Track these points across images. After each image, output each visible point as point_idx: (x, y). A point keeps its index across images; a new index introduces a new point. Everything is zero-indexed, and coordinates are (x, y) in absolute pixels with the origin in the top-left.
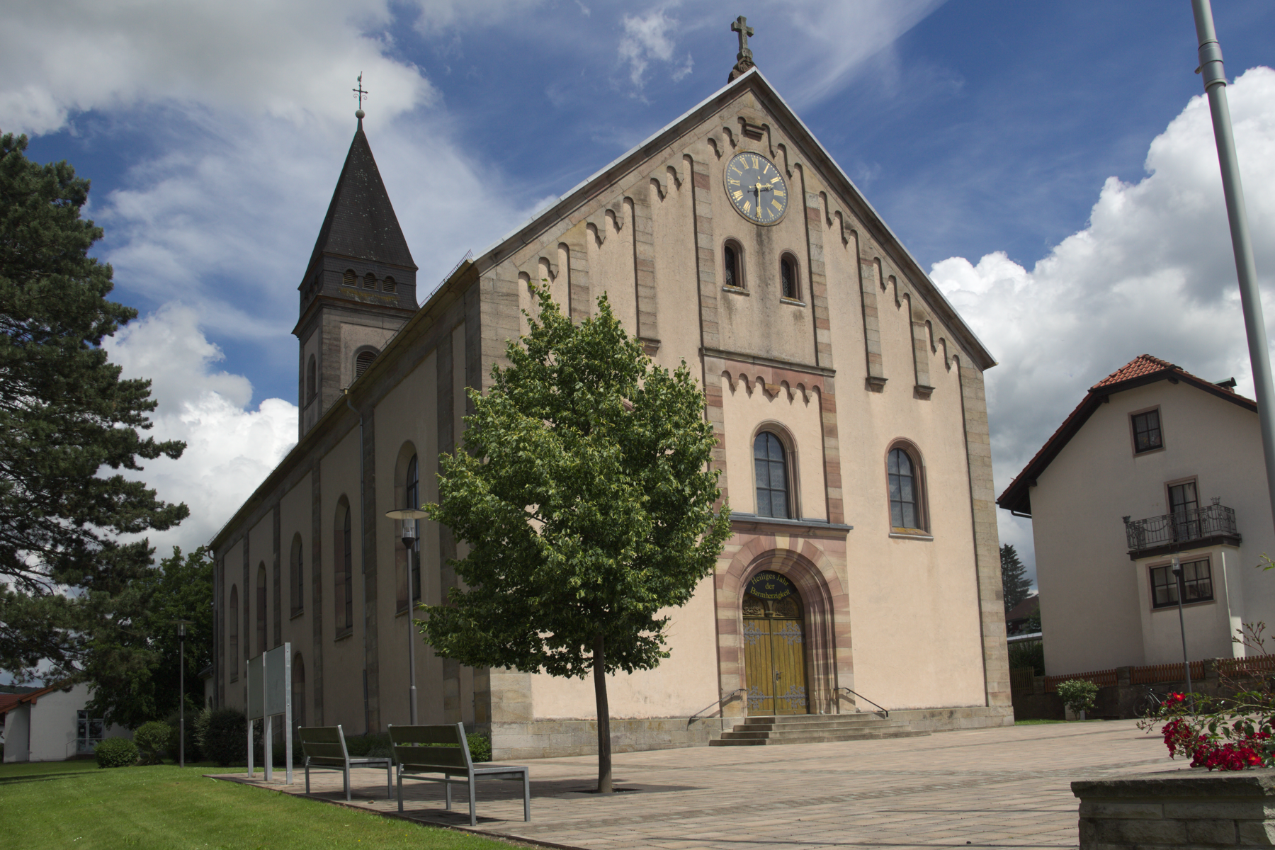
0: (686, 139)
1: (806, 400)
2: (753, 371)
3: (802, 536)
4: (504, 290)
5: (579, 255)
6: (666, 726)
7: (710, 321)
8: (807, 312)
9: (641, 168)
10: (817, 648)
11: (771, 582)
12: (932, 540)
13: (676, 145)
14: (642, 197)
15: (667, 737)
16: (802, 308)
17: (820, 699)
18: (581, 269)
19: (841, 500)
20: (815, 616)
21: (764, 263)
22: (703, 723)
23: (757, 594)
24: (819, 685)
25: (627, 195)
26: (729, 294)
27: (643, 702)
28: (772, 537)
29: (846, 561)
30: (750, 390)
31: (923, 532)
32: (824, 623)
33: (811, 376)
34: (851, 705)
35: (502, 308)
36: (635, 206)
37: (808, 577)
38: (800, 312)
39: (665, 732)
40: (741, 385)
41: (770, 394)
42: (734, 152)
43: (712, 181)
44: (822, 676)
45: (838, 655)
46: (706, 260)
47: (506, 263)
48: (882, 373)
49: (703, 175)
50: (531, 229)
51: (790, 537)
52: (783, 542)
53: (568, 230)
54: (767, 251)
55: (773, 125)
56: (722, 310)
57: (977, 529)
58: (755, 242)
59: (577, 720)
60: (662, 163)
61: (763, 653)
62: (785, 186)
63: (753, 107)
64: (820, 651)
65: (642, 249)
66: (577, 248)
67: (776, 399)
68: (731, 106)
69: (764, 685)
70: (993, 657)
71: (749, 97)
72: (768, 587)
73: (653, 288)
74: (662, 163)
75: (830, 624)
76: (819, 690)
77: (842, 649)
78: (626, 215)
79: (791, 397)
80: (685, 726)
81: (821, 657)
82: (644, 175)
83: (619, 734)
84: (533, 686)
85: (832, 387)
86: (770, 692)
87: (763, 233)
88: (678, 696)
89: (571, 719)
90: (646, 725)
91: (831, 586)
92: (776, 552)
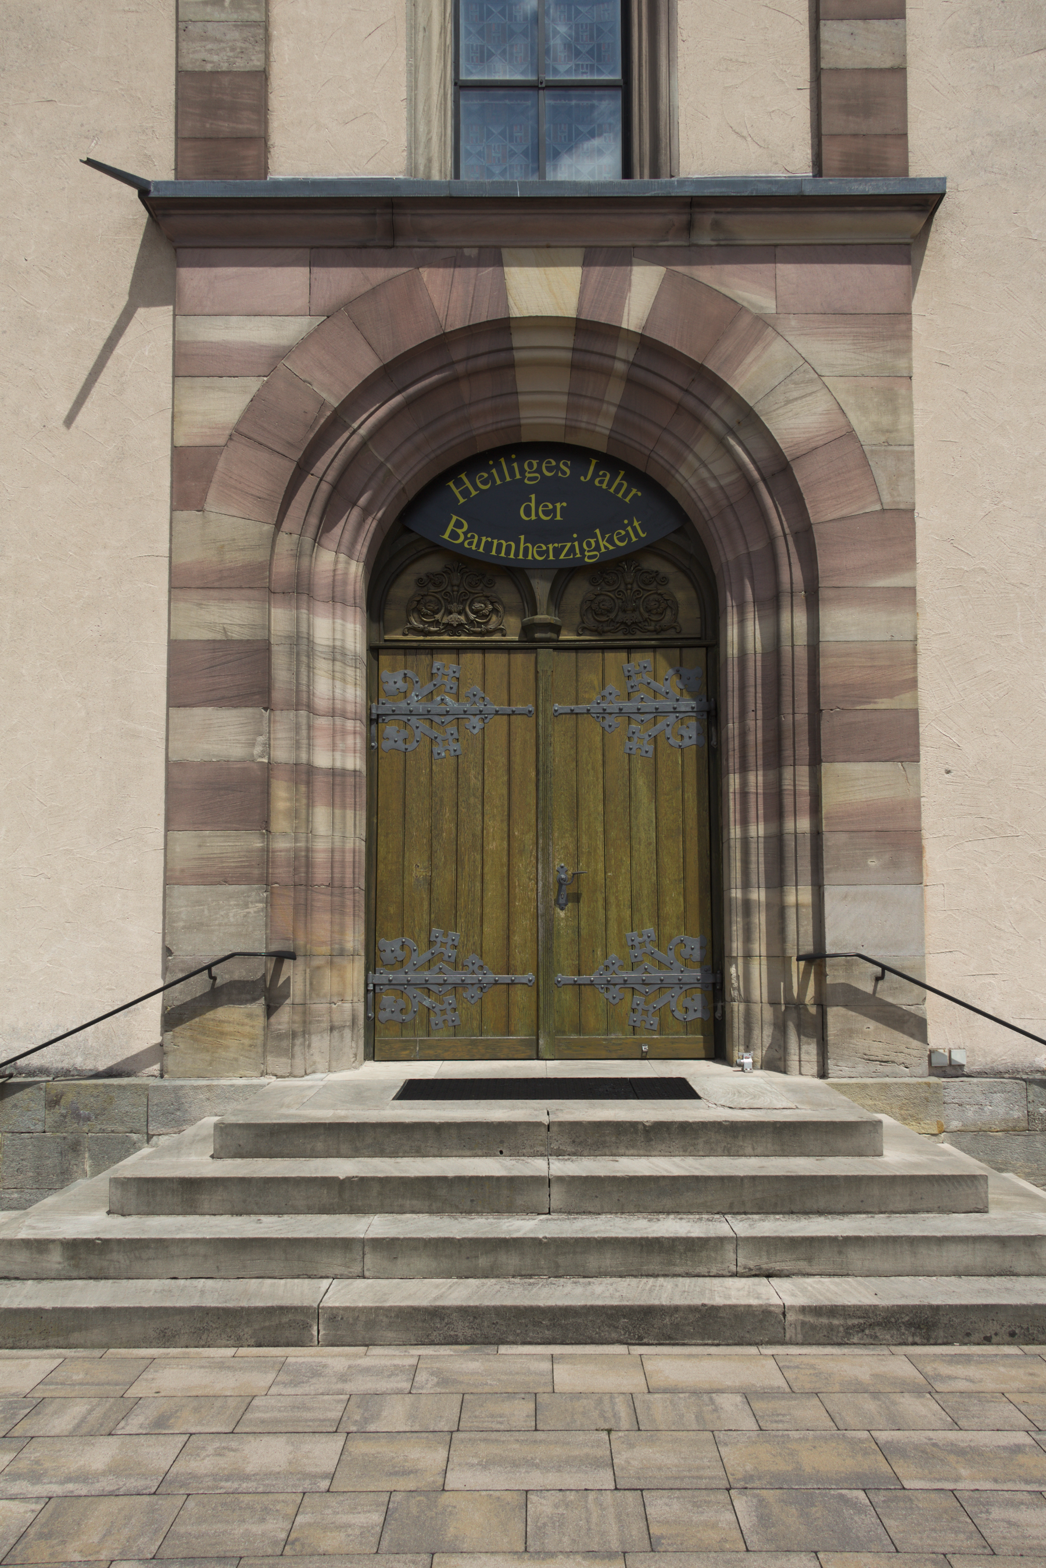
3: (652, 256)
10: (744, 769)
17: (747, 1000)
19: (900, 71)
20: (742, 622)
22: (53, 1102)
23: (475, 544)
24: (748, 939)
29: (907, 351)
32: (774, 653)
34: (902, 1039)
37: (704, 448)
44: (759, 895)
45: (832, 797)
61: (497, 790)
64: (757, 780)
69: (492, 930)
72: (533, 511)
75: (802, 654)
76: (748, 956)
77: (858, 768)
81: (757, 807)
86: (522, 955)
91: (802, 476)
92: (512, 324)
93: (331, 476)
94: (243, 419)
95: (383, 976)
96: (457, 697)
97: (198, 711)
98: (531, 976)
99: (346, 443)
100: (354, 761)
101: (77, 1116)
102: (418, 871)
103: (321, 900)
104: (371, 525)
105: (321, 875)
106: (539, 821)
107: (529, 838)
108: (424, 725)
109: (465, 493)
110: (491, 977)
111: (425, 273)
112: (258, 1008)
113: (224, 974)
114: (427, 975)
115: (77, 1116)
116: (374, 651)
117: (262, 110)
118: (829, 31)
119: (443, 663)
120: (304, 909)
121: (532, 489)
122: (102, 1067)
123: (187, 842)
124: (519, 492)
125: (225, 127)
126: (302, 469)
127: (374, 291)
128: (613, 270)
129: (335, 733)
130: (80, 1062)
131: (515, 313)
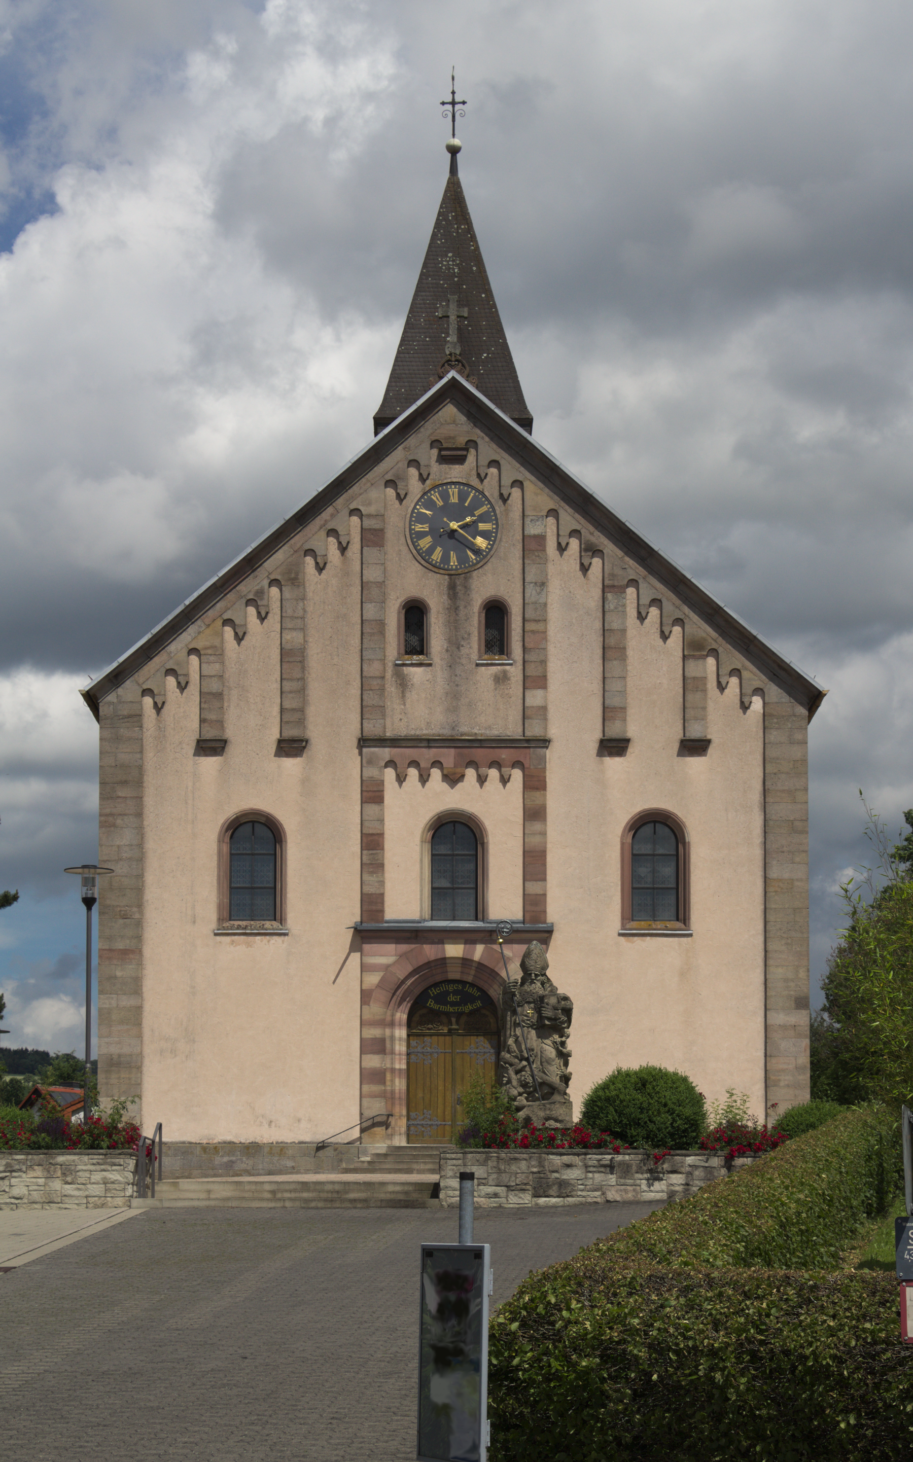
0: (355, 489)
1: (504, 781)
2: (426, 755)
3: (482, 942)
4: (125, 713)
5: (212, 658)
6: (290, 1152)
7: (373, 706)
8: (515, 672)
9: (292, 541)
11: (455, 993)
12: (691, 935)
13: (340, 502)
14: (293, 576)
15: (290, 1164)
16: (508, 668)
18: (213, 673)
19: (545, 895)
21: (456, 621)
22: (335, 1150)
23: (436, 1007)
25: (272, 577)
26: (404, 668)
27: (267, 1126)
28: (440, 946)
30: (424, 779)
31: (679, 925)
33: (512, 750)
35: (123, 732)
36: (284, 588)
38: (505, 673)
39: (288, 1158)
40: (413, 773)
41: (453, 779)
42: (424, 489)
43: (389, 534)
46: (372, 634)
47: (128, 684)
48: (625, 732)
49: (375, 530)
50: (157, 641)
51: (465, 943)
52: (454, 950)
53: (199, 633)
54: (461, 604)
55: (483, 438)
56: (391, 688)
57: (771, 917)
58: (445, 597)
59: (190, 1143)
60: (321, 528)
62: (495, 515)
63: (454, 422)
65: (289, 637)
66: (209, 652)
67: (460, 785)
68: (422, 430)
69: (440, 1111)
70: (782, 1084)
71: (449, 411)
72: (451, 998)
73: (302, 679)
74: (321, 528)
78: (274, 599)
79: (482, 780)
80: (313, 1153)
82: (296, 548)
83: (234, 1158)
84: (144, 1109)
85: (543, 759)
86: (448, 1117)
87: (458, 583)
88: (310, 1120)
89: (184, 1143)
90: (266, 1150)
92: (448, 961)
93: (400, 996)
94: (379, 982)
95: (411, 1122)
96: (431, 1048)
97: (369, 1056)
98: (450, 1123)
99: (404, 987)
100: (404, 1067)
101: (341, 1153)
102: (420, 1095)
103: (397, 1102)
104: (409, 1005)
105: (397, 1096)
106: (181, 1197)
107: (450, 1086)
108: (422, 1055)
109: (433, 993)
110: (440, 1123)
111: (424, 946)
112: (384, 1128)
113: (376, 1120)
114: (423, 1122)
115: (341, 1153)
116: (408, 1036)
117: (383, 903)
118: (527, 884)
119: (426, 1038)
120: (393, 1104)
121: (451, 992)
122: (346, 1142)
123: (366, 1088)
124: (447, 993)
125: (374, 908)
126: (394, 994)
127: (412, 950)
128: (472, 945)
129: (400, 1060)
130: (340, 1141)
131: (447, 956)
